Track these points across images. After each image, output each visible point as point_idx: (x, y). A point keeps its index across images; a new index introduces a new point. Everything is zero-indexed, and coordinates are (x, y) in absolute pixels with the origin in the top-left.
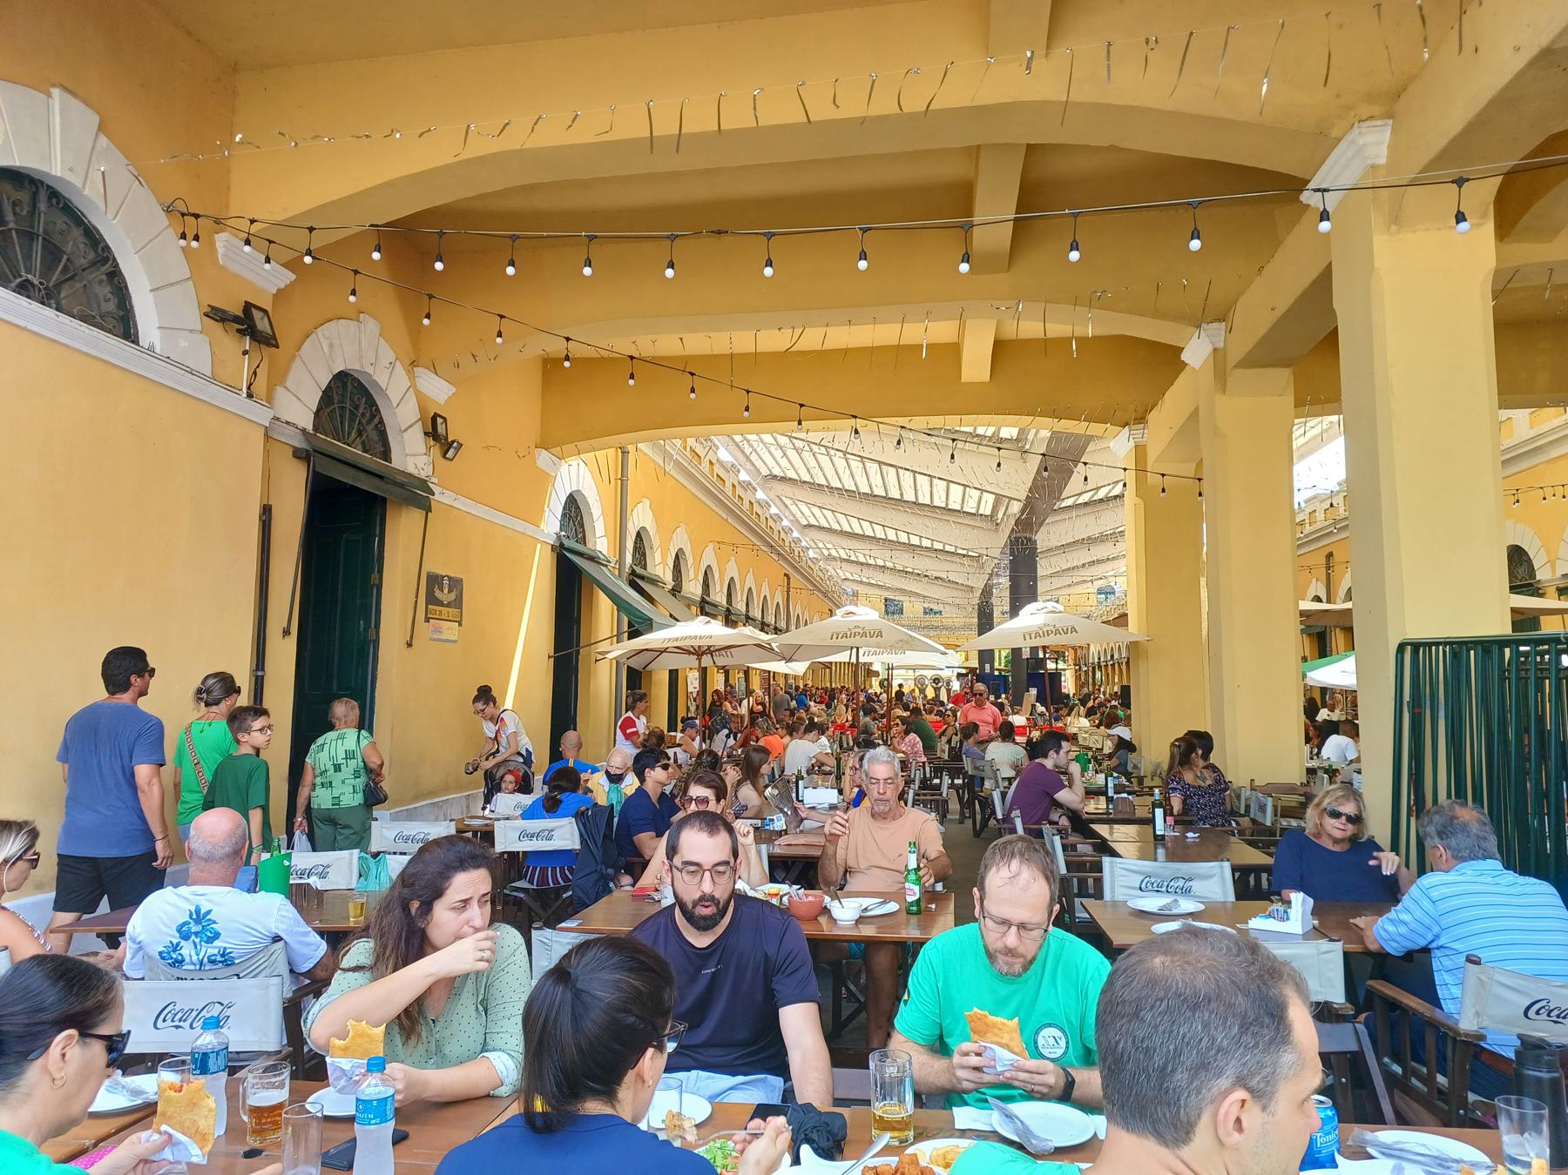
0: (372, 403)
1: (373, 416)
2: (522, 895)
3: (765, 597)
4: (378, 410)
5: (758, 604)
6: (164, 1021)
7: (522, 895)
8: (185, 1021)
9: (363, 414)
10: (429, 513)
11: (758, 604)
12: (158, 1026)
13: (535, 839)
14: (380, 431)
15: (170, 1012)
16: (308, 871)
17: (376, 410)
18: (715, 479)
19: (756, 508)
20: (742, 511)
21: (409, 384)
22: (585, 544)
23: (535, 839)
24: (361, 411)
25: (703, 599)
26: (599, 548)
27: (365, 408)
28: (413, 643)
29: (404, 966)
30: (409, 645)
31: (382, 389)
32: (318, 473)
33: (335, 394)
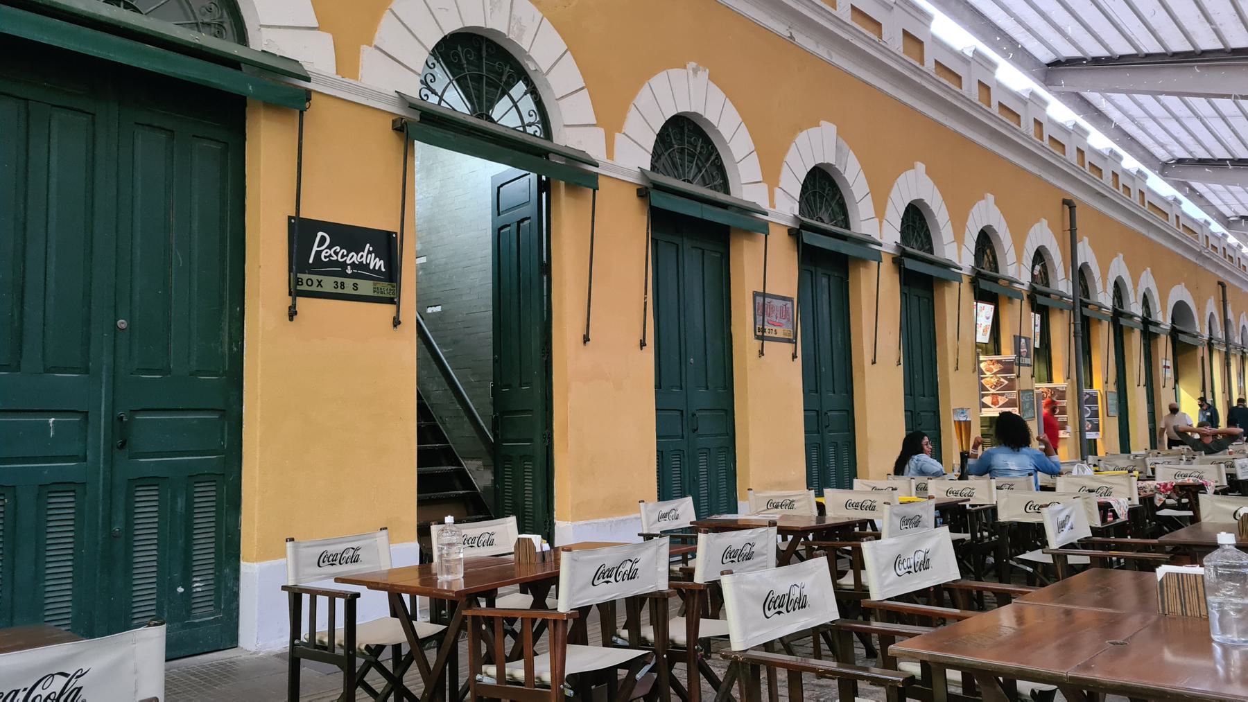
0: (708, 141)
1: (836, 194)
2: (1029, 569)
3: (1212, 315)
4: (714, 148)
5: (1238, 330)
6: (726, 558)
7: (1029, 569)
8: (782, 606)
9: (828, 195)
10: (881, 263)
11: (1238, 330)
12: (724, 562)
13: (612, 579)
14: (717, 166)
15: (771, 600)
16: (860, 504)
17: (712, 147)
18: (1181, 230)
19: (1122, 180)
20: (1131, 204)
21: (566, 48)
22: (1049, 287)
23: (612, 579)
24: (699, 149)
25: (1115, 310)
26: (1159, 319)
27: (702, 147)
28: (877, 361)
29: (835, 592)
30: (586, 339)
31: (526, 52)
32: (653, 206)
33: (673, 140)
